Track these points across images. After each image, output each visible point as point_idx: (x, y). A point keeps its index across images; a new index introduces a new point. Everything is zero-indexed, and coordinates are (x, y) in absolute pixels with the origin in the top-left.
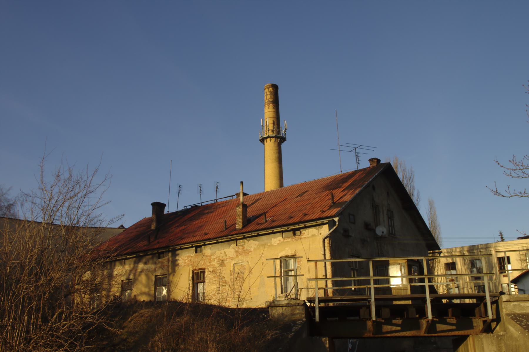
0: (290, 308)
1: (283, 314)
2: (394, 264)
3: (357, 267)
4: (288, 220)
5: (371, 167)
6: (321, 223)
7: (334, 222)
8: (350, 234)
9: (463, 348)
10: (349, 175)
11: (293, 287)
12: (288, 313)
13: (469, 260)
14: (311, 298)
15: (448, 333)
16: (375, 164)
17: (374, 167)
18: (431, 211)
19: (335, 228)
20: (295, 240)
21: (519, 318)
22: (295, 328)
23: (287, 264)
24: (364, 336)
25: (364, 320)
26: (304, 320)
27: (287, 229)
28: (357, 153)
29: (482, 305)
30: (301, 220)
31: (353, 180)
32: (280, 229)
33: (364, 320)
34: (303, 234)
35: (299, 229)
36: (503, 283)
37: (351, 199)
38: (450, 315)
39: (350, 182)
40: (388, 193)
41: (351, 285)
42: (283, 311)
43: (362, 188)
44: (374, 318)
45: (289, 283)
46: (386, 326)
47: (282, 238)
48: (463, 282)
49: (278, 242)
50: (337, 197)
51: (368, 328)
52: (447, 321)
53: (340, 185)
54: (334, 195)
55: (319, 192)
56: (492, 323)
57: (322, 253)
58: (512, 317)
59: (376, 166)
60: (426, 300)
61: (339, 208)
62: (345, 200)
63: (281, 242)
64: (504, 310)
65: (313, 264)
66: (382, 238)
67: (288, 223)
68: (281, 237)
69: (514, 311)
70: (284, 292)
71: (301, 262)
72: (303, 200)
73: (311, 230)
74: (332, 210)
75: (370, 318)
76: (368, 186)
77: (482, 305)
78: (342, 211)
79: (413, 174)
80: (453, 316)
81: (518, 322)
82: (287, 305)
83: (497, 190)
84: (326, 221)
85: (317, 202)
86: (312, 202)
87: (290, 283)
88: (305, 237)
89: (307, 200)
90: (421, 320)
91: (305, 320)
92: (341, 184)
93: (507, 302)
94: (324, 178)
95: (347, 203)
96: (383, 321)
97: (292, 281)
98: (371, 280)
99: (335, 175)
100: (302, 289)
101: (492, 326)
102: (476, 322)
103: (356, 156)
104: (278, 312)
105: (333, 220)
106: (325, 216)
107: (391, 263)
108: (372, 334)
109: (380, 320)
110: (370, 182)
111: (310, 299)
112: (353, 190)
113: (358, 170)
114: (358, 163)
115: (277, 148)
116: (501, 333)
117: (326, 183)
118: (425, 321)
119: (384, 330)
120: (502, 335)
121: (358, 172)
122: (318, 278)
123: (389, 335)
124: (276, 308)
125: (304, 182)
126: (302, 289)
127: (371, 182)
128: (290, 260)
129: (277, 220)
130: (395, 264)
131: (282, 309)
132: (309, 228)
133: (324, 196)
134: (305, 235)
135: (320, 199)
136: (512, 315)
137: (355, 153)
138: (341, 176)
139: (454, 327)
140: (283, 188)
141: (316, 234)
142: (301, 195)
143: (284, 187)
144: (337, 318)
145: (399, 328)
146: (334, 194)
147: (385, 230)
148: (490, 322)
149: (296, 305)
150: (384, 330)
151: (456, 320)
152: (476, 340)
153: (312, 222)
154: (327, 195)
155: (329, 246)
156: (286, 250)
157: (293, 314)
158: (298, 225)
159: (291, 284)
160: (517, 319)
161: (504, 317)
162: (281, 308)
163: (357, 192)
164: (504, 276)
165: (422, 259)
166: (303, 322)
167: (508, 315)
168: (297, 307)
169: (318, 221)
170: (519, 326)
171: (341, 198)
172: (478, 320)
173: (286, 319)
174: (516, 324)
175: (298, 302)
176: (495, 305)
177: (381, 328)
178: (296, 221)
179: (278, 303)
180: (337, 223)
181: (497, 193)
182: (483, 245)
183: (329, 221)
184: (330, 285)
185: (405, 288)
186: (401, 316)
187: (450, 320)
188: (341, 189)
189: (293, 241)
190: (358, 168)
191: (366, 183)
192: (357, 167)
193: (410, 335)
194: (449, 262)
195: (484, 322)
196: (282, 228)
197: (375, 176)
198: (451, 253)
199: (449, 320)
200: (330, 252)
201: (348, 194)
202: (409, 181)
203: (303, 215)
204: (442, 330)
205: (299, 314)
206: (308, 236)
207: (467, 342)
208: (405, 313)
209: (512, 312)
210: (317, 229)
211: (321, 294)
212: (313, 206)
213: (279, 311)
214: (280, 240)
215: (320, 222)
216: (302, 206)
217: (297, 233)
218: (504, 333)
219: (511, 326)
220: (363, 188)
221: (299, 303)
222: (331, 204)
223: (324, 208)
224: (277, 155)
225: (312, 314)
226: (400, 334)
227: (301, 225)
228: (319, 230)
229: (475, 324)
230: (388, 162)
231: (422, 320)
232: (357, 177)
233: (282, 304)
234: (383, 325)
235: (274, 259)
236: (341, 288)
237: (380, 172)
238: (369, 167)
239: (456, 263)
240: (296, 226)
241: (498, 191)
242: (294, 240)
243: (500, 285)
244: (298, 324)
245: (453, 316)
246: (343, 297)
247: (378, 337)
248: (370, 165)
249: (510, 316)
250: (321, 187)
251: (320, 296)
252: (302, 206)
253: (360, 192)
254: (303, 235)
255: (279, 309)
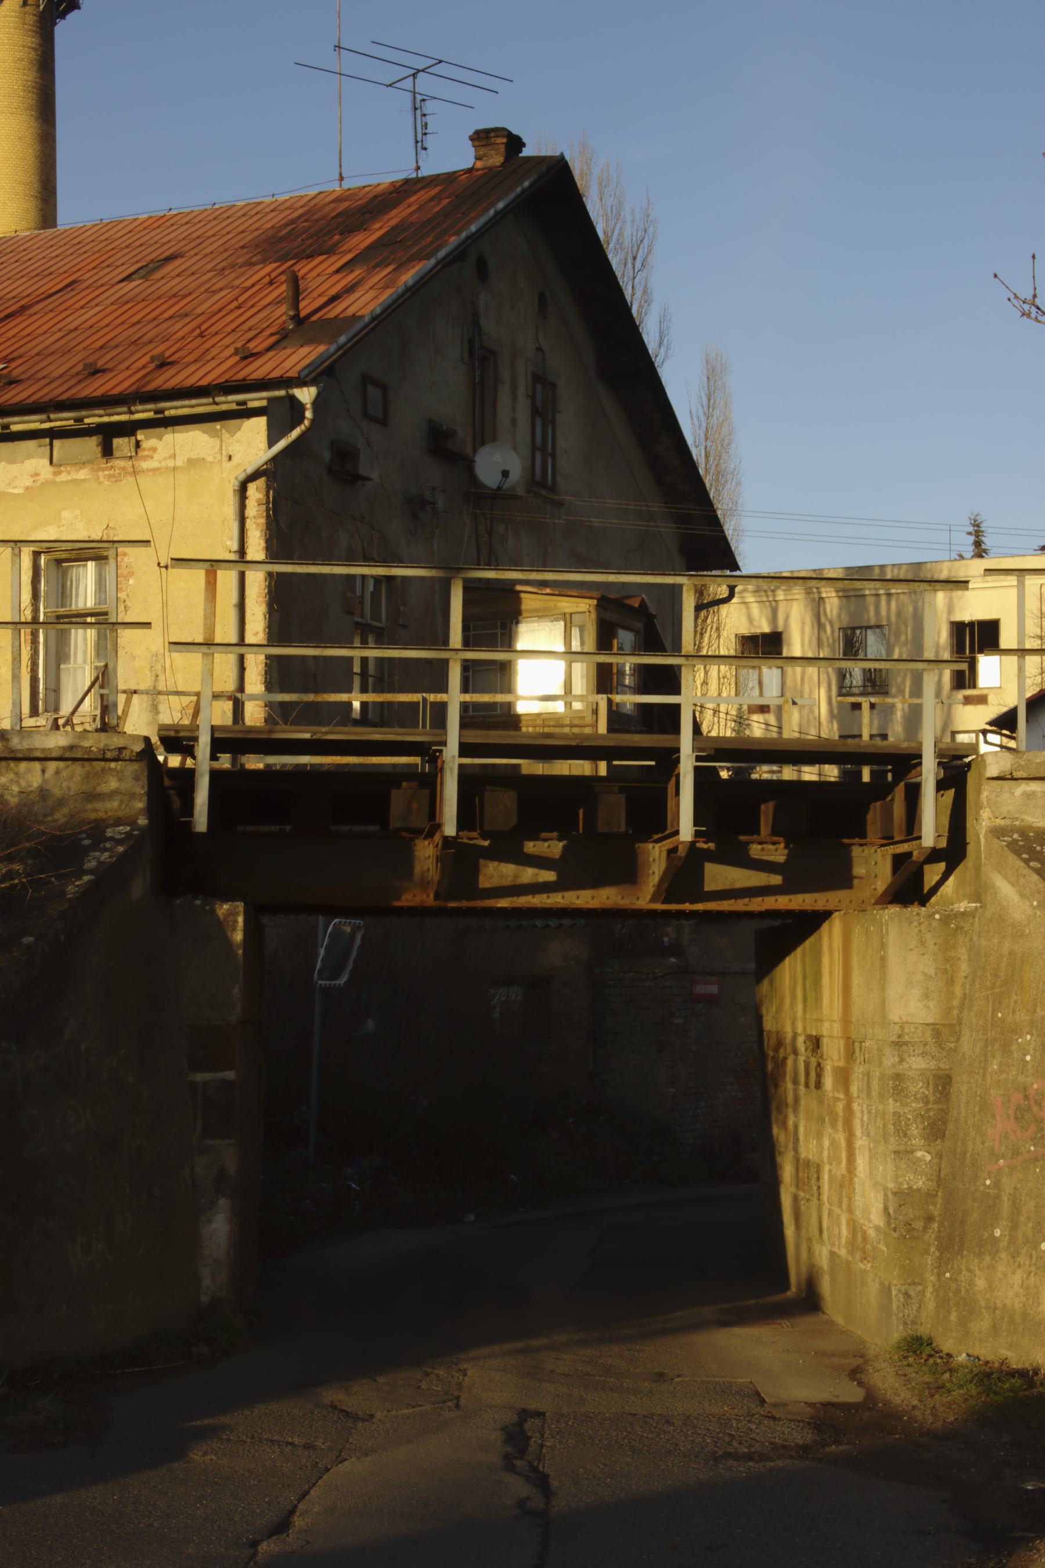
0: (78, 769)
1: (43, 793)
2: (539, 617)
3: (379, 620)
4: (80, 382)
5: (478, 170)
6: (234, 407)
7: (295, 408)
8: (363, 471)
9: (799, 968)
10: (375, 197)
11: (89, 690)
12: (69, 789)
13: (837, 626)
14: (176, 728)
15: (746, 900)
16: (496, 159)
17: (490, 169)
18: (709, 407)
19: (295, 433)
20: (110, 476)
21: (1038, 848)
22: (97, 854)
23: (64, 586)
24: (396, 904)
25: (404, 834)
26: (142, 821)
27: (71, 422)
28: (419, 98)
29: (900, 792)
30: (143, 387)
31: (392, 223)
32: (42, 422)
33: (404, 834)
34: (146, 453)
35: (128, 429)
36: (960, 729)
37: (378, 311)
38: (765, 828)
39: (378, 230)
40: (542, 298)
41: (350, 691)
42: (44, 781)
43: (432, 262)
44: (450, 829)
45: (68, 670)
46: (496, 864)
47: (47, 462)
48: (801, 716)
49: (28, 482)
50: (315, 294)
51: (418, 870)
52: (748, 855)
53: (331, 243)
54: (302, 284)
55: (233, 266)
56: (927, 868)
57: (229, 543)
58: (1015, 841)
59: (502, 165)
60: (677, 761)
61: (319, 343)
62: (350, 312)
63: (42, 484)
64: (985, 814)
65: (198, 576)
66: (498, 495)
67: (82, 395)
68: (44, 457)
69: (1022, 820)
70: (46, 711)
71: (131, 581)
72: (155, 296)
73: (185, 434)
74: (288, 351)
75: (438, 827)
76: (458, 256)
77: (900, 792)
78: (336, 361)
79: (651, 230)
80: (775, 832)
81: (1032, 864)
82: (67, 755)
83: (1035, 296)
84: (257, 400)
85: (220, 310)
86: (199, 310)
87: (75, 669)
88: (158, 469)
89: (174, 296)
90: (642, 845)
91: (146, 822)
92: (337, 237)
93: (1000, 782)
94: (259, 203)
95: (358, 326)
96: (486, 843)
97: (85, 662)
98: (451, 664)
99: (313, 192)
100: (135, 692)
101: (926, 878)
102: (867, 861)
103: (416, 109)
104: (23, 783)
105: (293, 399)
106: (255, 376)
107: (528, 611)
108: (432, 896)
109: (471, 839)
110: (468, 238)
111: (172, 734)
112: (391, 268)
113: (418, 180)
114: (420, 146)
115: (31, 41)
116: (962, 906)
117: (269, 225)
118: (660, 852)
119: (484, 883)
120: (964, 914)
121: (420, 185)
122: (217, 640)
123: (503, 903)
124: (12, 764)
125: (161, 214)
126: (135, 692)
127: (472, 237)
128: (81, 569)
129: (28, 379)
130: (543, 615)
131: (43, 771)
132: (176, 428)
133: (253, 285)
134: (156, 456)
135: (236, 299)
136: (1016, 836)
137: (409, 96)
138: (338, 200)
139: (776, 880)
140: (55, 230)
141: (210, 459)
142: (147, 271)
143: (59, 228)
144: (288, 828)
145: (550, 876)
146: (303, 278)
147: (516, 467)
148: (922, 859)
149: (109, 755)
150: (484, 883)
151: (786, 851)
152: (857, 930)
153: (194, 402)
154: (267, 279)
155: (265, 514)
156: (64, 522)
157: (92, 796)
158: (125, 409)
159: (79, 676)
160: (1031, 851)
161: (982, 841)
162: (37, 766)
163: (408, 277)
164: (968, 701)
165: (681, 586)
166: (136, 833)
167: (998, 832)
168: (113, 765)
169: (218, 399)
170: (1035, 877)
171: (334, 299)
172: (876, 851)
173: (57, 816)
174: (1027, 871)
175: (117, 741)
176: (951, 793)
177: (476, 872)
178: (116, 391)
179: (26, 745)
180: (308, 414)
181: (1034, 310)
182: (904, 568)
183: (270, 400)
184: (255, 684)
185: (577, 722)
186: (564, 827)
187: (763, 849)
188: (333, 259)
189: (100, 483)
190: (418, 168)
191: (453, 241)
192: (414, 166)
193: (594, 904)
194: (758, 631)
195: (899, 861)
196: (52, 416)
197: (492, 212)
198: (770, 593)
199: (759, 847)
200: (267, 541)
201: (367, 286)
202: (629, 265)
203: (152, 366)
204: (728, 887)
205: (119, 797)
206: (171, 463)
207: (820, 938)
208: (581, 812)
209: (1017, 823)
210: (215, 434)
211: (221, 714)
212: (203, 328)
213: (29, 777)
214: (37, 474)
215: (228, 402)
216: (150, 321)
217: (121, 444)
218: (974, 905)
219: (1006, 878)
220: (438, 263)
221: (124, 748)
222: (284, 323)
223: (249, 341)
224: (31, 76)
225: (177, 804)
226: (549, 901)
227: (140, 407)
228: (221, 441)
229: (859, 870)
230: (557, 154)
231: (650, 846)
232: (412, 209)
233: (44, 750)
234: (482, 861)
235: (15, 542)
236: (311, 697)
237: (518, 197)
238: (470, 171)
239: (784, 637)
240: (118, 414)
241: (1038, 302)
242: (102, 479)
243: (949, 734)
244: (112, 839)
245: (775, 832)
246: (323, 729)
247: (457, 911)
248: (473, 160)
249: (1006, 839)
250: (241, 244)
251: (217, 721)
252: (150, 321)
253: (412, 291)
254: (145, 458)
255: (29, 770)
